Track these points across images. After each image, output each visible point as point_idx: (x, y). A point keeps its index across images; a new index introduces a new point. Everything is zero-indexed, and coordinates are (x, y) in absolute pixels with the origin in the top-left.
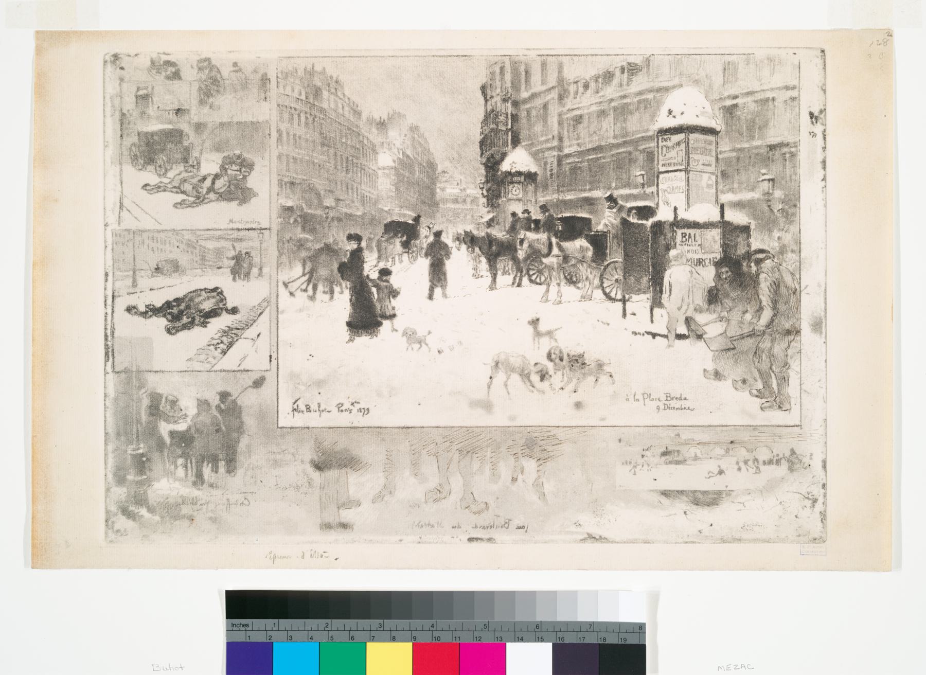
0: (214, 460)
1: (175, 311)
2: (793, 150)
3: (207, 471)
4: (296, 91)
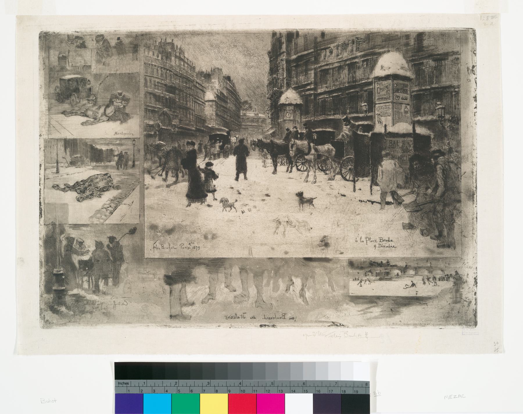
0: (106, 278)
1: (82, 187)
2: (457, 90)
3: (101, 284)
4: (156, 54)
